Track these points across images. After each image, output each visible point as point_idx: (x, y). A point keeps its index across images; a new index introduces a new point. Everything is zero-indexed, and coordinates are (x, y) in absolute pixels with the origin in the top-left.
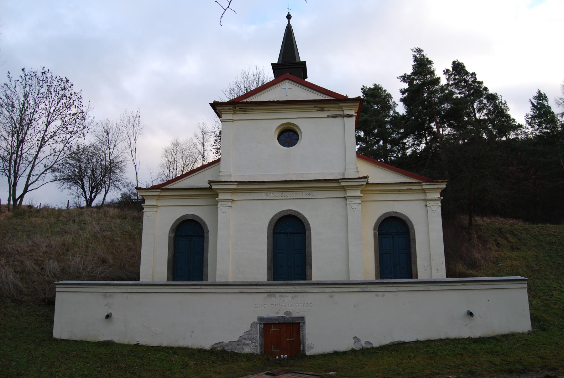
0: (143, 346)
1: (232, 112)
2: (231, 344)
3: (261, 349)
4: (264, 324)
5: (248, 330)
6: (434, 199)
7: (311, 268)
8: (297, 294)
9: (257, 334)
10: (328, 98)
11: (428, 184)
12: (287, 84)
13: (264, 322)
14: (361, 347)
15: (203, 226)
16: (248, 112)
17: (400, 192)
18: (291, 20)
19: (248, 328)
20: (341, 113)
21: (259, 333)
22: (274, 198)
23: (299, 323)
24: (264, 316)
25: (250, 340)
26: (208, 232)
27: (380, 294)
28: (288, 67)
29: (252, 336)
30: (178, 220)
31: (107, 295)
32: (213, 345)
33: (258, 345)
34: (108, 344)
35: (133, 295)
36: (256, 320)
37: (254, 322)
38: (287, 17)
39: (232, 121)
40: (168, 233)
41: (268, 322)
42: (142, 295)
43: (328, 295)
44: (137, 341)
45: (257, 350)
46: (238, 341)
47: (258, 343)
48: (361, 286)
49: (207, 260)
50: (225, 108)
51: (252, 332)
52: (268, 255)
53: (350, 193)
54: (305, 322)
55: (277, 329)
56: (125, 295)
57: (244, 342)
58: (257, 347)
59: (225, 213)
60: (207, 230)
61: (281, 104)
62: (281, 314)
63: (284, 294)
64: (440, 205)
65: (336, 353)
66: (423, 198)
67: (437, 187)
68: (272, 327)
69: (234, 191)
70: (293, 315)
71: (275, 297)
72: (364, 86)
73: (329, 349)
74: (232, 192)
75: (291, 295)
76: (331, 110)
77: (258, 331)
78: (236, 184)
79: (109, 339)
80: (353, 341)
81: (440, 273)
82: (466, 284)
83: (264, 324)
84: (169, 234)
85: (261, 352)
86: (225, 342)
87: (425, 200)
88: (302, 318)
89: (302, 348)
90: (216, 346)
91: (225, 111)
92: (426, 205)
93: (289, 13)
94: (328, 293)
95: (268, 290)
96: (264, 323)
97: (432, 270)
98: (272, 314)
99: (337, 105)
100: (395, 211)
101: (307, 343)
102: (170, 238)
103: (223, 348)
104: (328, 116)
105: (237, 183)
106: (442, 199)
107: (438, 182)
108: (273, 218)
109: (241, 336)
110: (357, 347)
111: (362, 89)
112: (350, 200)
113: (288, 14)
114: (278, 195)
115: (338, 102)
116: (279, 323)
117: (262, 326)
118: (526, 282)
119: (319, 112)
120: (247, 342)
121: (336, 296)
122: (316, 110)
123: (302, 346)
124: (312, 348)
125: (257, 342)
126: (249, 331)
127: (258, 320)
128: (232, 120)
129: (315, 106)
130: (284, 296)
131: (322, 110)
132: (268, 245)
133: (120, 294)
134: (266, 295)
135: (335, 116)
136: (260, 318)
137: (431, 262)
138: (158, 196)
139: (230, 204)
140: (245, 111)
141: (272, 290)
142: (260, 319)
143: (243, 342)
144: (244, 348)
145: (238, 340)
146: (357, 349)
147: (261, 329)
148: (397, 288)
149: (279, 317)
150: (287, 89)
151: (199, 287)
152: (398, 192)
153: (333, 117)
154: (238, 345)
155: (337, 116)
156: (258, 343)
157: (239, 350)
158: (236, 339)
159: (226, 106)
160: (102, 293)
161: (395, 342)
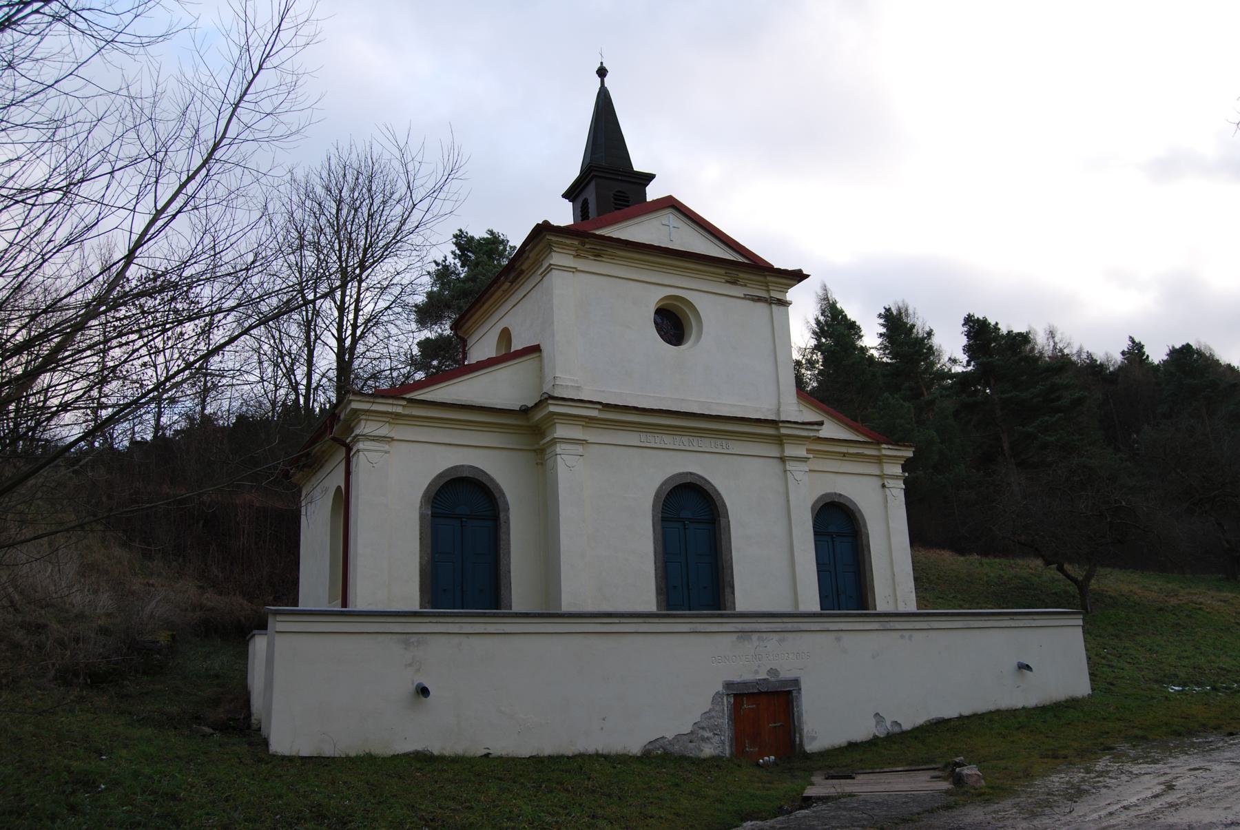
0: (500, 758)
1: (573, 253)
2: (678, 741)
3: (731, 746)
4: (735, 695)
5: (708, 710)
6: (894, 476)
7: (733, 593)
8: (786, 635)
9: (723, 717)
10: (741, 259)
11: (890, 447)
12: (671, 216)
13: (734, 692)
14: (886, 732)
15: (497, 496)
16: (603, 259)
17: (844, 458)
18: (606, 79)
19: (707, 705)
20: (763, 294)
21: (726, 715)
22: (642, 445)
23: (790, 692)
24: (735, 680)
25: (711, 731)
26: (509, 509)
27: (906, 634)
28: (620, 178)
29: (715, 721)
30: (440, 476)
31: (412, 640)
32: (645, 746)
33: (727, 740)
34: (423, 759)
35: (475, 641)
36: (720, 688)
37: (717, 693)
38: (597, 72)
39: (573, 272)
40: (418, 505)
41: (741, 692)
42: (496, 639)
43: (833, 635)
44: (485, 748)
45: (724, 749)
46: (692, 732)
47: (727, 735)
48: (881, 619)
49: (509, 572)
50: (564, 240)
51: (713, 713)
52: (655, 563)
53: (790, 451)
54: (800, 689)
55: (753, 704)
56: (456, 639)
57: (702, 736)
58: (724, 743)
59: (572, 469)
60: (506, 503)
61: (675, 256)
62: (763, 675)
63: (764, 635)
64: (904, 487)
65: (852, 746)
66: (878, 473)
67: (901, 455)
68: (745, 702)
69: (589, 422)
70: (780, 677)
71: (751, 639)
72: (460, 230)
73: (840, 740)
74: (584, 423)
75: (776, 637)
76: (748, 285)
77: (726, 711)
78: (596, 408)
79: (419, 747)
80: (873, 722)
81: (909, 603)
82: (1015, 617)
83: (735, 695)
84: (421, 507)
85: (732, 753)
86: (667, 737)
87: (882, 476)
88: (796, 682)
89: (797, 739)
90: (651, 747)
91: (561, 246)
92: (883, 486)
93: (602, 63)
94: (833, 633)
95: (740, 627)
96: (733, 694)
97: (898, 601)
98: (748, 677)
99: (761, 279)
100: (838, 492)
101: (805, 731)
102: (422, 517)
103: (664, 749)
104: (746, 297)
105: (600, 407)
106: (906, 477)
107: (905, 446)
108: (661, 486)
109: (695, 724)
110: (881, 733)
111: (455, 236)
112: (792, 463)
113: (599, 65)
114: (668, 441)
115: (767, 273)
116: (760, 693)
117: (732, 700)
118: (1081, 617)
119: (728, 285)
120: (707, 734)
121: (846, 637)
122: (723, 281)
123: (797, 735)
124: (814, 738)
125: (723, 734)
126: (710, 710)
127: (724, 687)
128: (574, 270)
129: (726, 273)
130: (765, 638)
131: (734, 282)
132: (654, 543)
133: (443, 639)
134: (735, 636)
135: (756, 298)
136: (727, 684)
137: (895, 589)
138: (393, 416)
139: (580, 449)
140: (598, 256)
141: (747, 627)
142: (728, 685)
143: (699, 736)
144: (702, 748)
145: (692, 731)
146: (882, 736)
147: (729, 706)
148: (929, 623)
149: (759, 680)
150: (671, 227)
151: (616, 620)
152: (841, 458)
153: (753, 300)
154: (691, 742)
155: (759, 299)
156: (727, 735)
157: (694, 752)
158: (687, 729)
159: (566, 238)
160: (398, 636)
161: (933, 719)
